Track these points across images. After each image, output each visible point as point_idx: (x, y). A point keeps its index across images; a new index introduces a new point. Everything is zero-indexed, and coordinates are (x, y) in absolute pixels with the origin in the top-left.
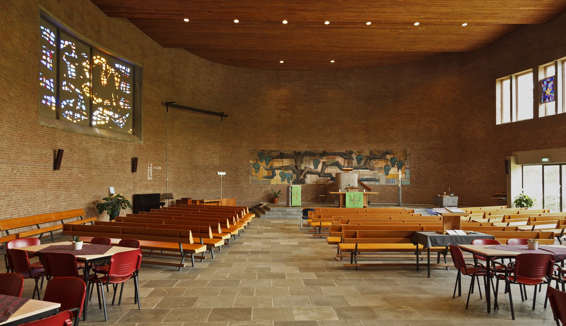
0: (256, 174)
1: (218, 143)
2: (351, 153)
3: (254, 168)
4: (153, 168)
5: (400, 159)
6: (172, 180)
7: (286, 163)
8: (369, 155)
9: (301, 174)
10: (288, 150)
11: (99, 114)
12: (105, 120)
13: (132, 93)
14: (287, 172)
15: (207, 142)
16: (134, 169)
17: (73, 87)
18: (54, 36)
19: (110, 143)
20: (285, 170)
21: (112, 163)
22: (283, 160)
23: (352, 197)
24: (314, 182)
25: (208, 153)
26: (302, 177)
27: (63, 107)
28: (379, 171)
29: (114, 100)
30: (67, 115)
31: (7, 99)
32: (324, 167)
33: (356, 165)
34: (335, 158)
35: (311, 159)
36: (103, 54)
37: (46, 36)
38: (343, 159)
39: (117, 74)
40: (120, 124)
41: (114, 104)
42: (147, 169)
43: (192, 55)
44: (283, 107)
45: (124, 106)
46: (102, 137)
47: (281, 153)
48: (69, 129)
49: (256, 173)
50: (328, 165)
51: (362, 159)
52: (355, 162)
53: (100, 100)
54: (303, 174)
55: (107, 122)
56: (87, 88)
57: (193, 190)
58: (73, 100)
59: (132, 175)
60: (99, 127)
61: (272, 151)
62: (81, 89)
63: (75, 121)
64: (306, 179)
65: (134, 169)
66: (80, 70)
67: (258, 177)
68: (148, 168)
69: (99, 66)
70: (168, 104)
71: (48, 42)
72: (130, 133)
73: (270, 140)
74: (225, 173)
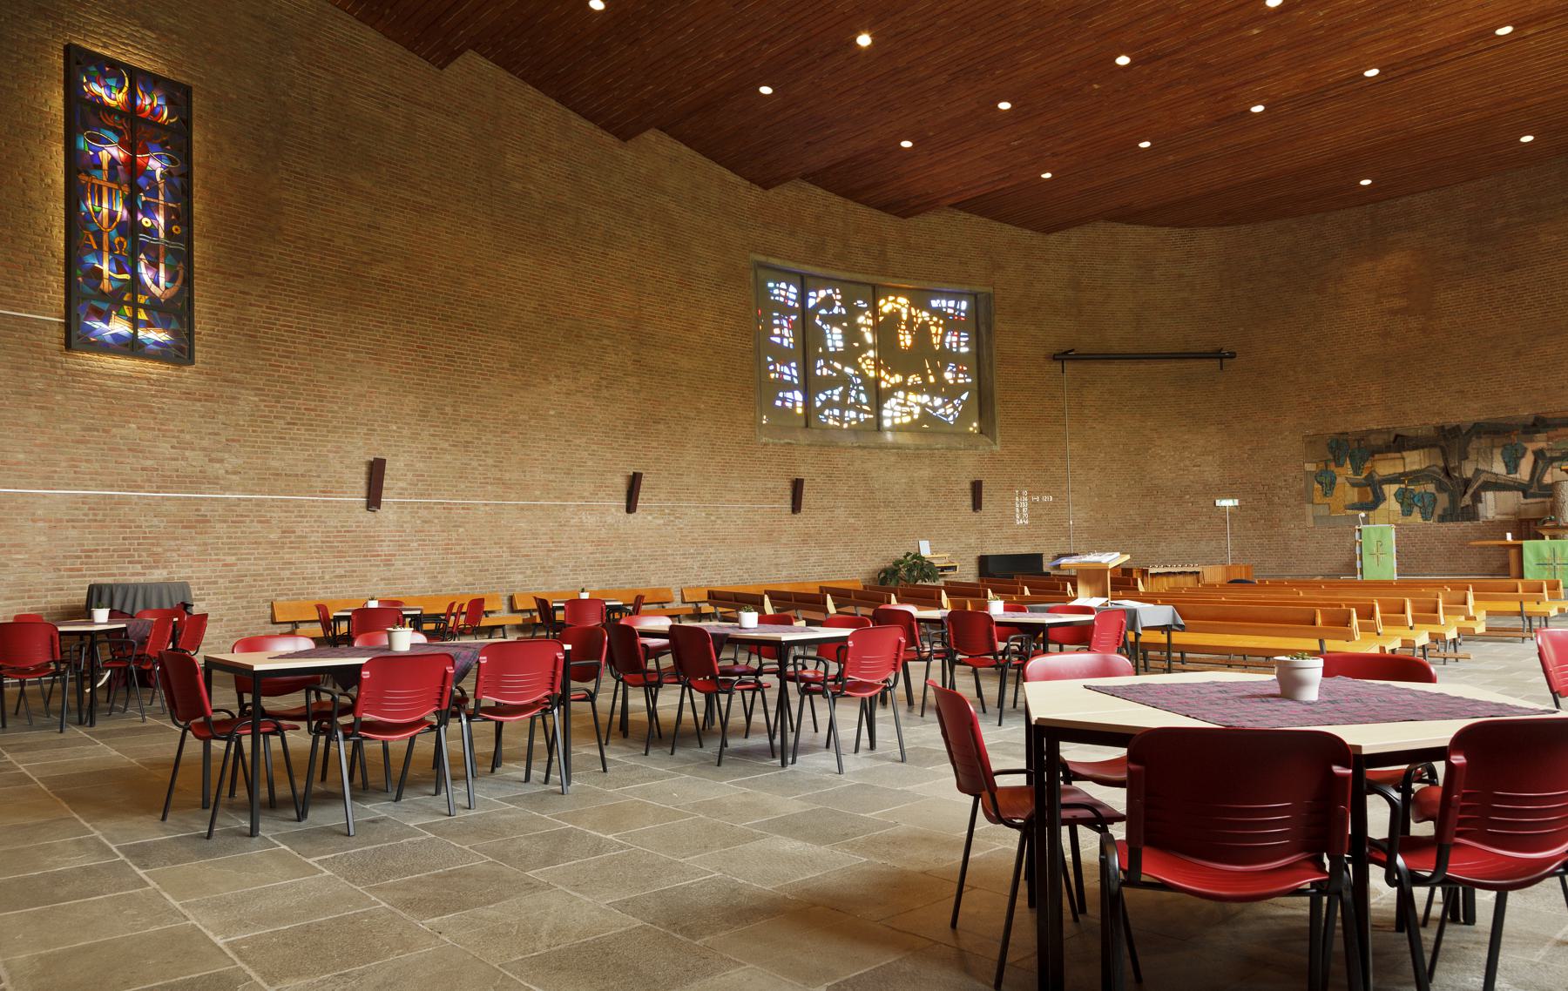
0: (1327, 500)
3: (1318, 482)
4: (1030, 499)
6: (1085, 524)
9: (1465, 493)
10: (1417, 421)
11: (898, 404)
12: (910, 413)
13: (974, 350)
14: (1418, 489)
15: (1183, 428)
16: (977, 505)
17: (838, 365)
18: (795, 291)
19: (918, 456)
20: (1411, 482)
21: (923, 495)
22: (1405, 454)
23: (1547, 554)
24: (1507, 514)
25: (1186, 454)
26: (1467, 500)
27: (818, 404)
29: (929, 371)
30: (827, 417)
31: (692, 415)
32: (1540, 462)
36: (898, 291)
37: (780, 295)
39: (935, 319)
40: (947, 416)
41: (932, 379)
42: (1014, 502)
43: (1129, 228)
44: (1398, 303)
45: (955, 379)
46: (899, 448)
48: (828, 441)
49: (1325, 495)
50: (1553, 460)
53: (898, 378)
54: (1470, 491)
55: (916, 417)
56: (868, 361)
57: (1149, 545)
58: (841, 389)
59: (975, 517)
60: (896, 429)
61: (1371, 432)
62: (857, 366)
63: (845, 426)
64: (1480, 505)
65: (977, 505)
66: (852, 334)
67: (1332, 508)
68: (1017, 499)
69: (894, 317)
70: (1062, 357)
71: (785, 304)
72: (973, 433)
73: (1363, 403)
74: (1236, 502)
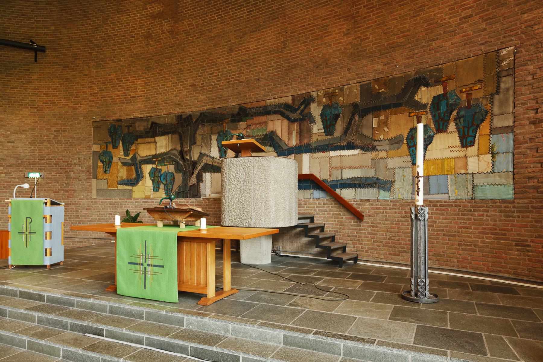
0: (106, 176)
1: (27, 110)
2: (307, 101)
3: (101, 161)
5: (469, 95)
7: (161, 147)
8: (358, 100)
9: (193, 173)
14: (164, 169)
26: (193, 180)
28: (392, 152)
33: (320, 138)
34: (266, 123)
35: (214, 132)
38: (286, 122)
47: (153, 123)
51: (337, 117)
52: (318, 128)
54: (196, 172)
61: (136, 119)
64: (201, 184)
73: (132, 94)
